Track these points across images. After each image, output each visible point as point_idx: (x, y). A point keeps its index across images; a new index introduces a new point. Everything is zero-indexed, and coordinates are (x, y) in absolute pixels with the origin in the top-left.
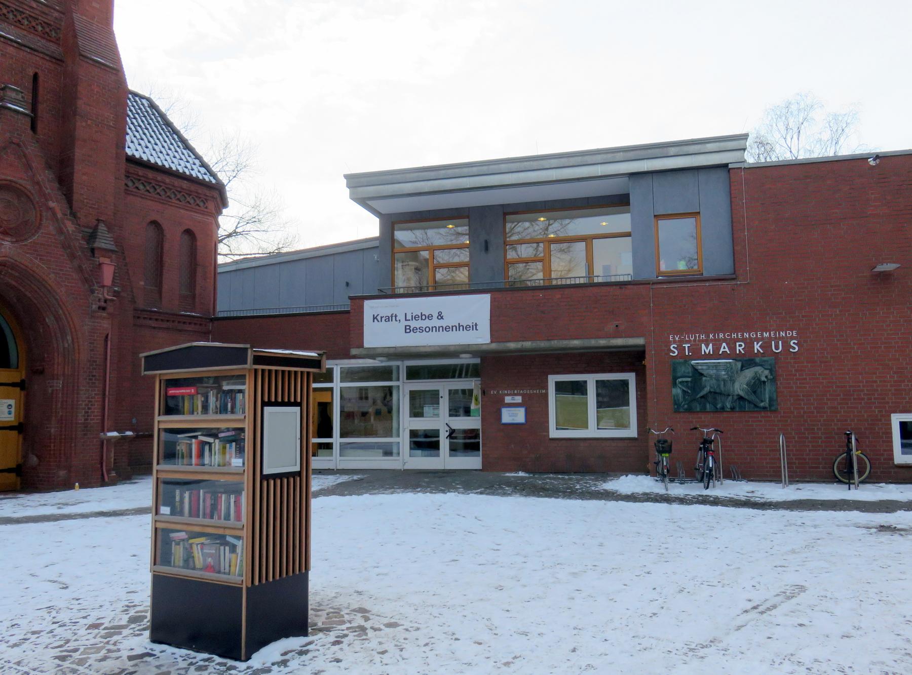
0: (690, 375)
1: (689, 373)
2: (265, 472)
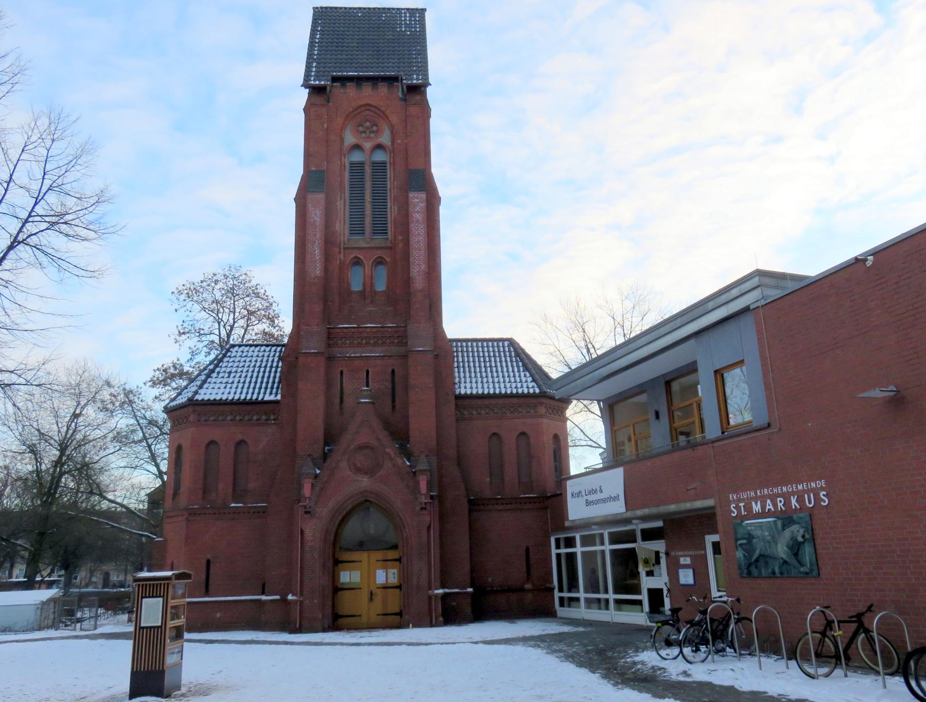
2: (142, 625)
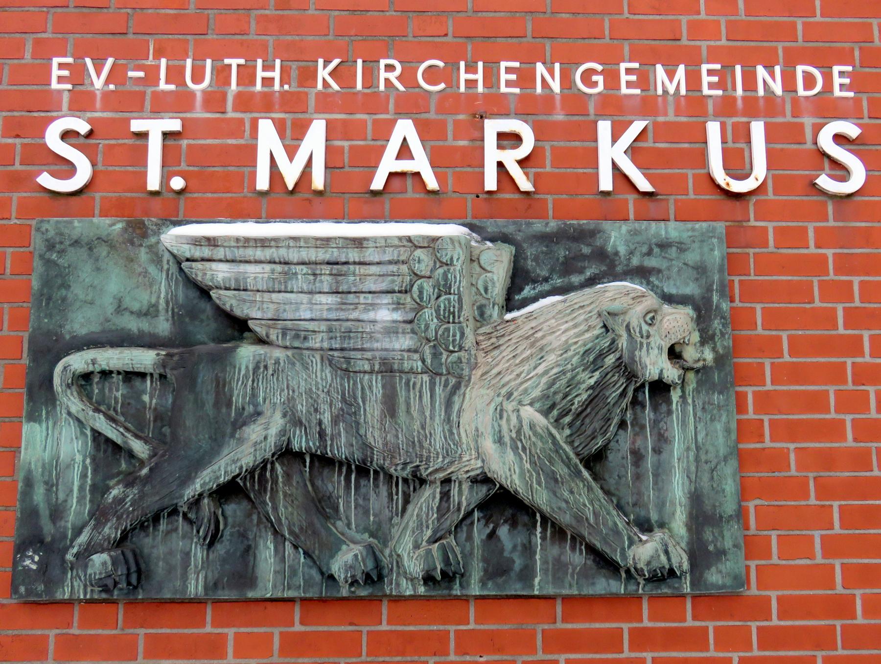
1: (150, 312)
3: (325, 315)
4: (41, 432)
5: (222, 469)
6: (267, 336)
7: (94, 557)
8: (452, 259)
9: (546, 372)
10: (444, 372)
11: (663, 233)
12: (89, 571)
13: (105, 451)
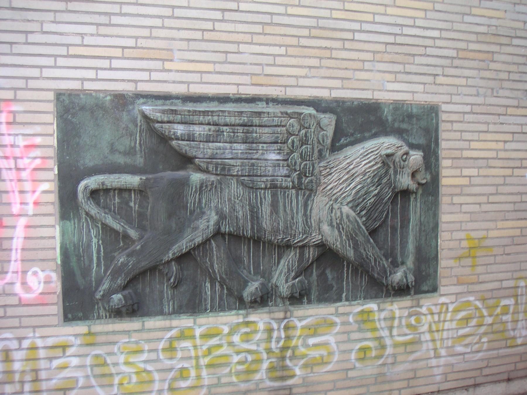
0: (139, 160)
1: (130, 152)
3: (240, 156)
4: (71, 226)
5: (184, 244)
6: (207, 168)
7: (113, 296)
8: (310, 125)
9: (354, 188)
10: (304, 188)
11: (410, 110)
12: (111, 304)
13: (110, 236)
